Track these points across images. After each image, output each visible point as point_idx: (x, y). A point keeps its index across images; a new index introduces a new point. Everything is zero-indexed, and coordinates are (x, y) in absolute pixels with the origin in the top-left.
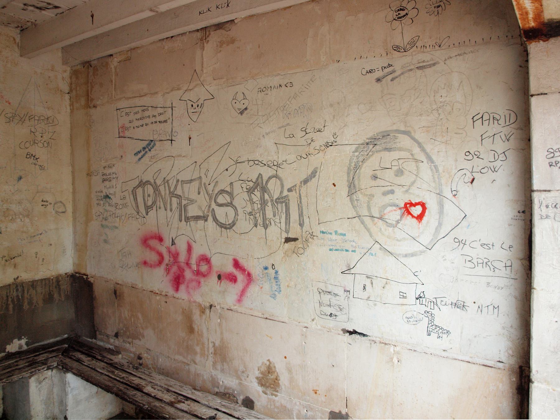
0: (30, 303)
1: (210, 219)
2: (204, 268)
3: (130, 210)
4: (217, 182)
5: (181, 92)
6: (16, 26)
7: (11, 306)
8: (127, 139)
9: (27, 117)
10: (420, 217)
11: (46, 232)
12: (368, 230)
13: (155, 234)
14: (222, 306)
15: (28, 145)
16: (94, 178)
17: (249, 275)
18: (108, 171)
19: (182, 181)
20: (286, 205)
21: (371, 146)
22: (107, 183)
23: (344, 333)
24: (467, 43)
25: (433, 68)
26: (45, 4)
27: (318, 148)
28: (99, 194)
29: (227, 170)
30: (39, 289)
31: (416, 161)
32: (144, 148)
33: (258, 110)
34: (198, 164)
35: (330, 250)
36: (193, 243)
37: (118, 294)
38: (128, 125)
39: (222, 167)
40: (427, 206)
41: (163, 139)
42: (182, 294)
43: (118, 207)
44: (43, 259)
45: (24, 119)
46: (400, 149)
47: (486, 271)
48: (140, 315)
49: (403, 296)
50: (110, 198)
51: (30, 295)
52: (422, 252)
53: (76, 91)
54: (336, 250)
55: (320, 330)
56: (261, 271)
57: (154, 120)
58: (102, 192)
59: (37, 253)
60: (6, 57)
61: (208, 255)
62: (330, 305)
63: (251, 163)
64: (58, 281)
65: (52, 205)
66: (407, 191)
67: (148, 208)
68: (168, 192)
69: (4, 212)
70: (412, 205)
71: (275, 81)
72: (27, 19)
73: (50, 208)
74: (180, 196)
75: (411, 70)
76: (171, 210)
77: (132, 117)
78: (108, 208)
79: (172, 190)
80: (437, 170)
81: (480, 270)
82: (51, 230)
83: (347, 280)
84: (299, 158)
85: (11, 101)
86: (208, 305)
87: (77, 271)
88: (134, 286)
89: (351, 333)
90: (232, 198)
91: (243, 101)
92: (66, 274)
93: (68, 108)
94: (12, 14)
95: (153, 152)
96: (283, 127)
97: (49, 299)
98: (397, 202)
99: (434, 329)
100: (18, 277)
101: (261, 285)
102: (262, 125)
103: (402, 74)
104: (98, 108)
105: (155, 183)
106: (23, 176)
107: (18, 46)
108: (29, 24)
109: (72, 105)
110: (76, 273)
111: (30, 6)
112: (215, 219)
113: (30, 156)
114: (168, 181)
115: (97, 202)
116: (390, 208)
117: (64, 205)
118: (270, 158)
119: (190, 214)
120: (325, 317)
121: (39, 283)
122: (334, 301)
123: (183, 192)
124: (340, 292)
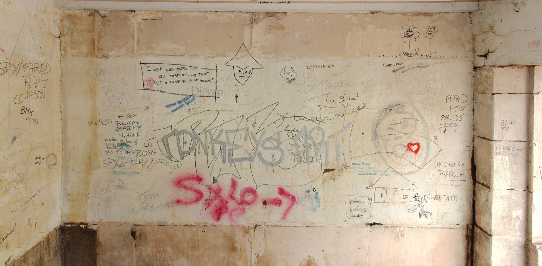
1: (257, 159)
2: (249, 197)
3: (158, 156)
4: (264, 131)
5: (228, 59)
10: (416, 152)
12: (385, 160)
14: (267, 224)
19: (226, 131)
20: (326, 146)
21: (388, 111)
24: (445, 56)
25: (426, 68)
27: (352, 110)
29: (275, 122)
31: (415, 120)
32: (180, 102)
35: (359, 175)
36: (238, 180)
39: (272, 118)
40: (420, 145)
42: (225, 220)
46: (406, 113)
49: (406, 197)
52: (417, 171)
55: (350, 227)
57: (193, 78)
61: (254, 186)
62: (358, 210)
63: (298, 118)
66: (409, 137)
68: (209, 139)
70: (412, 144)
74: (224, 142)
75: (414, 68)
76: (213, 154)
77: (163, 72)
80: (427, 125)
84: (337, 116)
86: (252, 226)
89: (371, 225)
90: (279, 144)
95: (191, 105)
99: (424, 213)
101: (303, 204)
113: (25, 110)
116: (398, 147)
118: (315, 116)
119: (235, 156)
120: (354, 218)
122: (361, 206)
123: (228, 140)
124: (365, 200)
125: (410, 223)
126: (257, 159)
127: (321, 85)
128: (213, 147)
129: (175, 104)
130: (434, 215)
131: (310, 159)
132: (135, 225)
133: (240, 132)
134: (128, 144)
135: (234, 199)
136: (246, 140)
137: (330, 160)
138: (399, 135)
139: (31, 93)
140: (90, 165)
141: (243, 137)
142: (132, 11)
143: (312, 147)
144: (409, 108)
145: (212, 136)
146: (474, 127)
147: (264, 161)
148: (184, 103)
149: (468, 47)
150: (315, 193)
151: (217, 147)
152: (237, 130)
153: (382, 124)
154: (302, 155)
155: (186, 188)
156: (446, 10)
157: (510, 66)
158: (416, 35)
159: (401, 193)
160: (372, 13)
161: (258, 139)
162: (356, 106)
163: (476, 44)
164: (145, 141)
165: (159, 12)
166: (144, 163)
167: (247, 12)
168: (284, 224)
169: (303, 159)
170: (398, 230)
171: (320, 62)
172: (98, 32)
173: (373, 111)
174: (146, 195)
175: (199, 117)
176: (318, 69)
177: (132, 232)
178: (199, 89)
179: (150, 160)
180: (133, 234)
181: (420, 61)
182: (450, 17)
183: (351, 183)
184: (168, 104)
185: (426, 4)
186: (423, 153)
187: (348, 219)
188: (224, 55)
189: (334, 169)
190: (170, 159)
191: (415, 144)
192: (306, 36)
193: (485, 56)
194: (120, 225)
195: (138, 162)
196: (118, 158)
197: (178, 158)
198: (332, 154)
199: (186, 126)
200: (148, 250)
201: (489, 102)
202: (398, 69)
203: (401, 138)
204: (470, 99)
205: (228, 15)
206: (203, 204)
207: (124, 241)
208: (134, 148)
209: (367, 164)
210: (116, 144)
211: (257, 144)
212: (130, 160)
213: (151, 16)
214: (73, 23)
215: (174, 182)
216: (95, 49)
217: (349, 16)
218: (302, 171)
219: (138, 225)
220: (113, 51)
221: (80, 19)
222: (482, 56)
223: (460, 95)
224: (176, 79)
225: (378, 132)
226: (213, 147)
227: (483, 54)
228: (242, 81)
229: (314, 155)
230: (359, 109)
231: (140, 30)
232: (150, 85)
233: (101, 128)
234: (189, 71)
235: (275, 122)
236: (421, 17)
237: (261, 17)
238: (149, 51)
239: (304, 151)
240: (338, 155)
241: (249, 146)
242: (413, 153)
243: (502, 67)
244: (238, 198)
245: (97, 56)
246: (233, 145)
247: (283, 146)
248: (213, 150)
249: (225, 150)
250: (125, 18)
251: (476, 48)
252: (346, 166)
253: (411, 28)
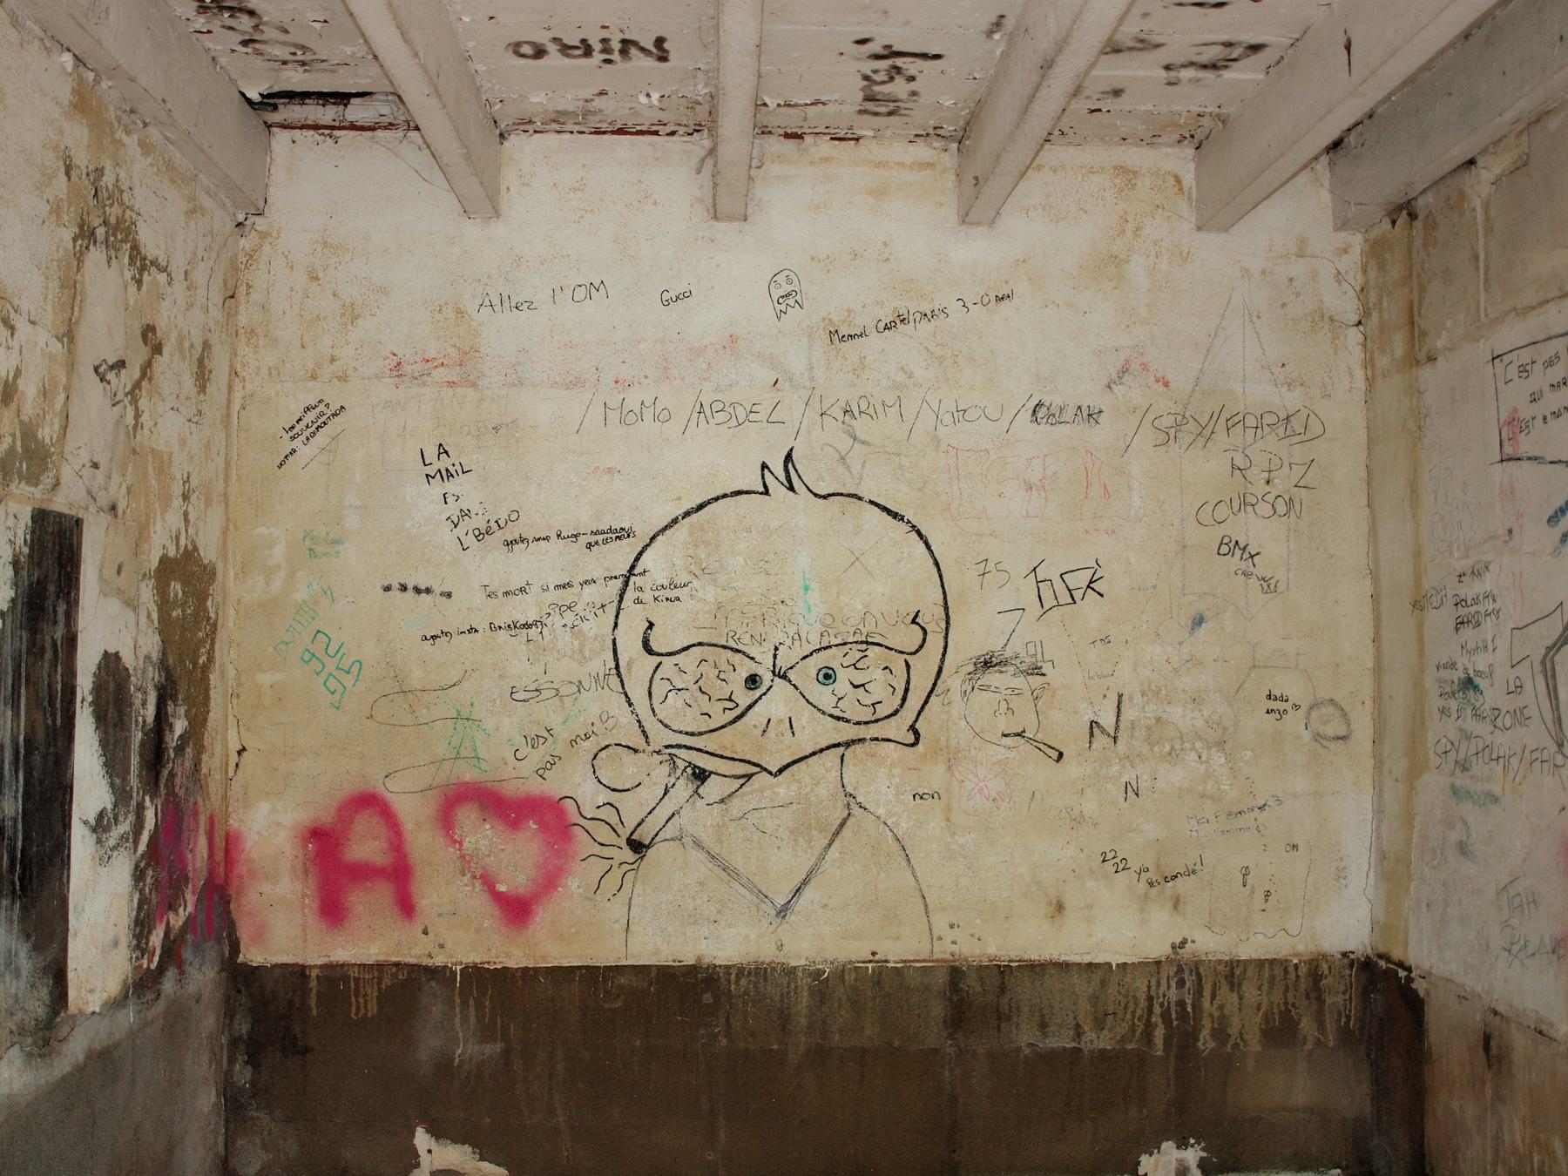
0: (1220, 1034)
6: (1178, 137)
7: (1159, 1033)
8: (1525, 464)
9: (1222, 421)
11: (1279, 801)
15: (1222, 512)
16: (1431, 614)
18: (1472, 589)
22: (1468, 633)
26: (1219, 48)
28: (1446, 674)
30: (1250, 992)
37: (1494, 1051)
38: (1526, 412)
43: (1499, 722)
44: (1267, 894)
45: (1210, 428)
50: (1476, 688)
51: (1221, 1007)
53: (1381, 310)
58: (1453, 665)
59: (1246, 872)
60: (1156, 243)
64: (1315, 976)
65: (1302, 712)
69: (1148, 728)
72: (1195, 109)
73: (1294, 721)
78: (1471, 725)
82: (1296, 796)
85: (1169, 377)
87: (1381, 950)
88: (1544, 1028)
92: (1344, 955)
93: (1359, 373)
94: (1149, 107)
97: (1281, 1031)
100: (1184, 942)
104: (1440, 362)
106: (1207, 614)
107: (1190, 198)
108: (1207, 122)
109: (1368, 363)
110: (1380, 956)
111: (1183, 66)
113: (1231, 547)
115: (1440, 703)
117: (1344, 714)
121: (1250, 973)
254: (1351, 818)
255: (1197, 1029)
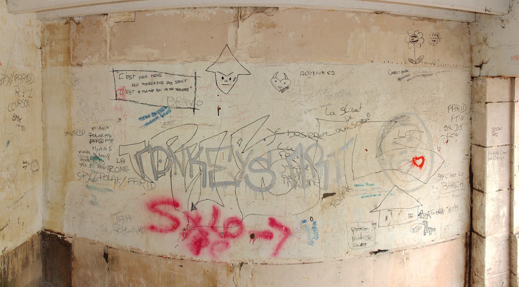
1: (243, 184)
2: (233, 229)
3: (131, 174)
4: (252, 150)
5: (209, 64)
10: (421, 166)
12: (390, 179)
13: (168, 199)
14: (255, 262)
17: (287, 229)
19: (207, 149)
20: (325, 167)
21: (393, 123)
23: (371, 254)
24: (447, 65)
25: (431, 77)
27: (355, 123)
29: (265, 139)
31: (420, 131)
32: (154, 114)
33: (300, 90)
34: (229, 134)
35: (362, 197)
36: (221, 207)
38: (129, 88)
39: (261, 135)
40: (425, 158)
41: (182, 107)
42: (205, 255)
46: (411, 125)
47: (453, 189)
48: (142, 281)
49: (411, 216)
52: (421, 186)
54: (367, 196)
55: (352, 259)
56: (299, 225)
57: (169, 86)
61: (239, 216)
62: (361, 238)
63: (292, 134)
66: (414, 151)
67: (157, 175)
68: (187, 158)
70: (417, 159)
71: (318, 68)
74: (204, 163)
75: (419, 76)
76: (191, 176)
77: (135, 80)
79: (193, 156)
80: (431, 137)
81: (450, 189)
83: (375, 217)
84: (338, 131)
86: (238, 263)
89: (376, 253)
90: (270, 165)
91: (285, 81)
95: (167, 118)
96: (324, 106)
98: (408, 158)
99: (428, 230)
101: (299, 237)
102: (304, 103)
103: (414, 77)
105: (169, 149)
106: (10, 140)
112: (248, 183)
113: (16, 118)
114: (187, 148)
116: (403, 163)
118: (312, 131)
119: (217, 180)
120: (357, 247)
122: (364, 233)
123: (209, 160)
124: (369, 226)
125: (415, 243)
126: (243, 184)
127: (319, 94)
128: (191, 167)
129: (149, 116)
130: (438, 230)
131: (307, 183)
132: (108, 246)
133: (223, 151)
134: (100, 158)
135: (216, 231)
136: (230, 160)
137: (330, 183)
138: (404, 149)
139: (20, 102)
140: (66, 177)
141: (226, 157)
142: (104, 14)
143: (309, 168)
144: (414, 120)
145: (190, 155)
146: (471, 136)
147: (252, 187)
148: (158, 115)
149: (467, 56)
150: (312, 222)
151: (196, 169)
152: (219, 149)
153: (387, 138)
154: (297, 178)
155: (161, 213)
156: (448, 17)
157: (499, 77)
158: (421, 41)
159: (406, 213)
160: (377, 13)
161: (244, 160)
162: (359, 119)
163: (473, 54)
164: (118, 156)
165: (132, 12)
166: (117, 180)
167: (232, 8)
168: (275, 262)
169: (298, 183)
170: (403, 254)
171: (318, 68)
172: (73, 40)
173: (378, 123)
174: (118, 215)
175: (175, 132)
176: (317, 76)
177: (104, 253)
178: (175, 100)
179: (123, 178)
180: (106, 256)
181: (425, 69)
182: (452, 25)
183: (354, 208)
184: (142, 117)
185: (431, 9)
186: (428, 166)
187: (350, 250)
188: (204, 60)
189: (335, 194)
190: (143, 178)
191: (420, 158)
192: (302, 36)
193: (480, 66)
194: (93, 243)
195: (110, 178)
196: (91, 172)
197: (153, 179)
198: (333, 175)
199: (160, 141)
200: (120, 277)
201: (483, 111)
202: (403, 77)
203: (406, 152)
204: (468, 109)
205: (209, 11)
206: (180, 234)
207: (97, 261)
208: (107, 163)
209: (371, 185)
210: (90, 157)
211: (244, 166)
212: (102, 175)
213: (123, 18)
214: (52, 33)
215: (148, 205)
216: (71, 59)
217: (351, 15)
218: (297, 197)
219: (111, 248)
220: (87, 59)
221: (57, 29)
222: (477, 66)
223: (460, 105)
224: (150, 87)
225: (382, 148)
226: (191, 167)
227: (478, 65)
228: (226, 89)
229: (311, 177)
230: (362, 122)
231: (113, 35)
232: (123, 94)
233: (76, 139)
234: (164, 78)
235: (265, 139)
236: (426, 22)
237: (248, 13)
238: (122, 57)
239: (299, 174)
240: (339, 176)
241: (233, 167)
242: (418, 168)
243: (493, 77)
244: (221, 229)
245: (72, 65)
246: (215, 166)
247: (274, 168)
248: (191, 171)
249: (206, 172)
250: (98, 23)
251: (473, 59)
252: (348, 189)
253: (416, 33)
254: (36, 192)
255: (8, 275)
